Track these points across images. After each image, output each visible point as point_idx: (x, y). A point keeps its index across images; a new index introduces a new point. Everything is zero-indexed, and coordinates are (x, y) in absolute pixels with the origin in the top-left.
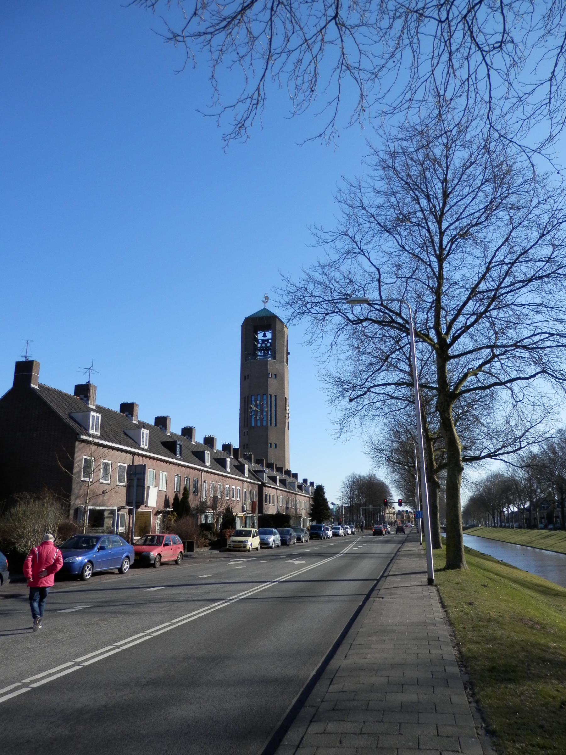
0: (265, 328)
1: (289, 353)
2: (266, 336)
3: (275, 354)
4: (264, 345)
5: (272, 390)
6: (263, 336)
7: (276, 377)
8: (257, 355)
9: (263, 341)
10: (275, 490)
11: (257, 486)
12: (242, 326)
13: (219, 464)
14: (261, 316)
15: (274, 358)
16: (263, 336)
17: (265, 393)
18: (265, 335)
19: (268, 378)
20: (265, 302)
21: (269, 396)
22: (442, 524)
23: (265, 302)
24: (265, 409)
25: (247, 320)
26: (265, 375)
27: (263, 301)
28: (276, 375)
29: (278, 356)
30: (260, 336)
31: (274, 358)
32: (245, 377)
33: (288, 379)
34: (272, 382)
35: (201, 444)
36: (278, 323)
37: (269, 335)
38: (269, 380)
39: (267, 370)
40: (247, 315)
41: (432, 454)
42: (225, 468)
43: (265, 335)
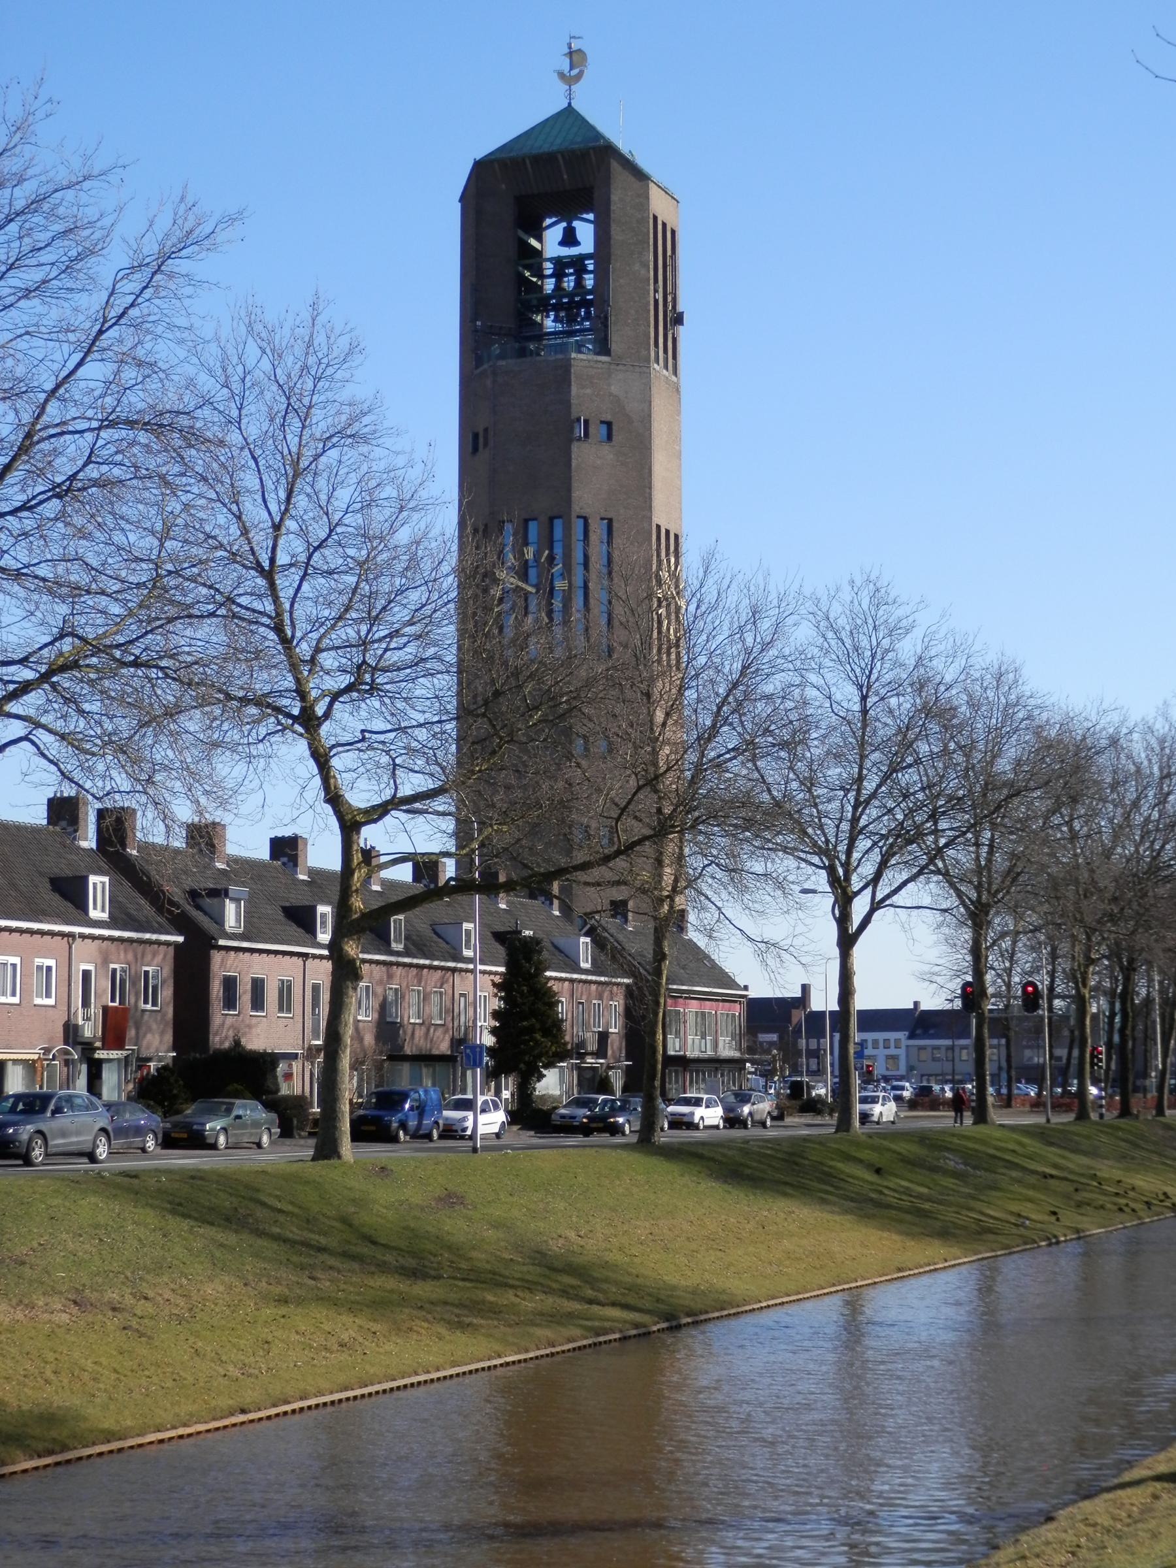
0: (570, 204)
1: (678, 320)
2: (576, 243)
3: (606, 326)
4: (569, 283)
5: (587, 496)
6: (563, 243)
7: (609, 437)
8: (539, 335)
9: (561, 265)
10: (300, 961)
11: (171, 950)
12: (463, 199)
13: (65, 896)
14: (546, 148)
15: (603, 347)
16: (563, 243)
17: (560, 510)
18: (569, 239)
19: (570, 440)
20: (569, 80)
21: (578, 525)
22: (875, 1043)
23: (569, 80)
24: (560, 585)
25: (482, 169)
26: (560, 430)
27: (562, 75)
28: (609, 425)
29: (617, 343)
30: (551, 243)
31: (603, 347)
32: (476, 436)
33: (677, 439)
34: (592, 463)
35: (34, 830)
36: (620, 183)
37: (585, 231)
38: (575, 447)
39: (567, 404)
40: (481, 152)
41: (352, 874)
42: (82, 906)
43: (569, 239)
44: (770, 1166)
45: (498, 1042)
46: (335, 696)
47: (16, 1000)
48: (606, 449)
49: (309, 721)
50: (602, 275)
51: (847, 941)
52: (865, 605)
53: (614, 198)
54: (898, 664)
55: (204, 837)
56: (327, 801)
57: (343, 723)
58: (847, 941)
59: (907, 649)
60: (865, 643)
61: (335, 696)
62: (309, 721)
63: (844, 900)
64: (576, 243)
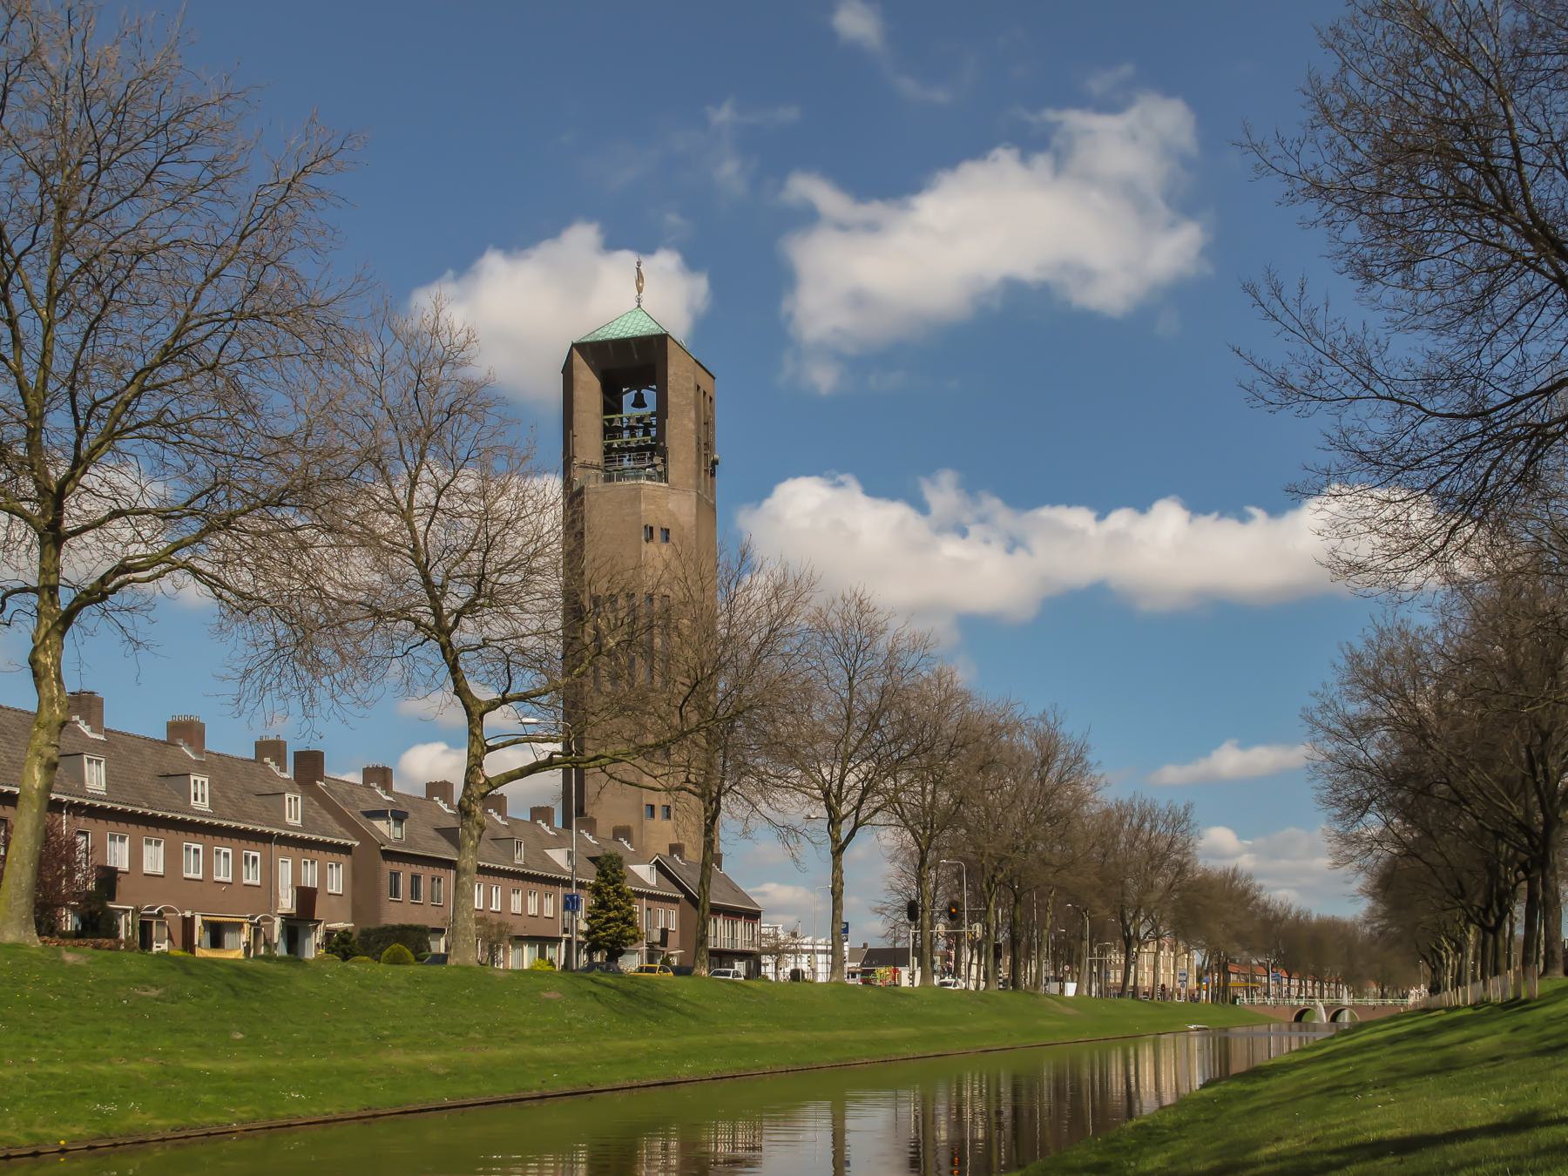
2: (644, 405)
28: (667, 531)
37: (650, 396)
44: (978, 980)
45: (692, 262)
46: (460, 613)
47: (200, 876)
48: (664, 547)
49: (441, 631)
50: (661, 428)
51: (838, 851)
52: (852, 613)
53: (671, 371)
54: (875, 655)
55: (380, 775)
56: (456, 693)
57: (466, 634)
58: (838, 851)
59: (882, 644)
60: (852, 640)
61: (460, 613)
62: (441, 631)
63: (834, 821)
64: (644, 405)
